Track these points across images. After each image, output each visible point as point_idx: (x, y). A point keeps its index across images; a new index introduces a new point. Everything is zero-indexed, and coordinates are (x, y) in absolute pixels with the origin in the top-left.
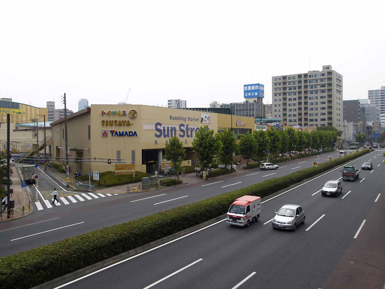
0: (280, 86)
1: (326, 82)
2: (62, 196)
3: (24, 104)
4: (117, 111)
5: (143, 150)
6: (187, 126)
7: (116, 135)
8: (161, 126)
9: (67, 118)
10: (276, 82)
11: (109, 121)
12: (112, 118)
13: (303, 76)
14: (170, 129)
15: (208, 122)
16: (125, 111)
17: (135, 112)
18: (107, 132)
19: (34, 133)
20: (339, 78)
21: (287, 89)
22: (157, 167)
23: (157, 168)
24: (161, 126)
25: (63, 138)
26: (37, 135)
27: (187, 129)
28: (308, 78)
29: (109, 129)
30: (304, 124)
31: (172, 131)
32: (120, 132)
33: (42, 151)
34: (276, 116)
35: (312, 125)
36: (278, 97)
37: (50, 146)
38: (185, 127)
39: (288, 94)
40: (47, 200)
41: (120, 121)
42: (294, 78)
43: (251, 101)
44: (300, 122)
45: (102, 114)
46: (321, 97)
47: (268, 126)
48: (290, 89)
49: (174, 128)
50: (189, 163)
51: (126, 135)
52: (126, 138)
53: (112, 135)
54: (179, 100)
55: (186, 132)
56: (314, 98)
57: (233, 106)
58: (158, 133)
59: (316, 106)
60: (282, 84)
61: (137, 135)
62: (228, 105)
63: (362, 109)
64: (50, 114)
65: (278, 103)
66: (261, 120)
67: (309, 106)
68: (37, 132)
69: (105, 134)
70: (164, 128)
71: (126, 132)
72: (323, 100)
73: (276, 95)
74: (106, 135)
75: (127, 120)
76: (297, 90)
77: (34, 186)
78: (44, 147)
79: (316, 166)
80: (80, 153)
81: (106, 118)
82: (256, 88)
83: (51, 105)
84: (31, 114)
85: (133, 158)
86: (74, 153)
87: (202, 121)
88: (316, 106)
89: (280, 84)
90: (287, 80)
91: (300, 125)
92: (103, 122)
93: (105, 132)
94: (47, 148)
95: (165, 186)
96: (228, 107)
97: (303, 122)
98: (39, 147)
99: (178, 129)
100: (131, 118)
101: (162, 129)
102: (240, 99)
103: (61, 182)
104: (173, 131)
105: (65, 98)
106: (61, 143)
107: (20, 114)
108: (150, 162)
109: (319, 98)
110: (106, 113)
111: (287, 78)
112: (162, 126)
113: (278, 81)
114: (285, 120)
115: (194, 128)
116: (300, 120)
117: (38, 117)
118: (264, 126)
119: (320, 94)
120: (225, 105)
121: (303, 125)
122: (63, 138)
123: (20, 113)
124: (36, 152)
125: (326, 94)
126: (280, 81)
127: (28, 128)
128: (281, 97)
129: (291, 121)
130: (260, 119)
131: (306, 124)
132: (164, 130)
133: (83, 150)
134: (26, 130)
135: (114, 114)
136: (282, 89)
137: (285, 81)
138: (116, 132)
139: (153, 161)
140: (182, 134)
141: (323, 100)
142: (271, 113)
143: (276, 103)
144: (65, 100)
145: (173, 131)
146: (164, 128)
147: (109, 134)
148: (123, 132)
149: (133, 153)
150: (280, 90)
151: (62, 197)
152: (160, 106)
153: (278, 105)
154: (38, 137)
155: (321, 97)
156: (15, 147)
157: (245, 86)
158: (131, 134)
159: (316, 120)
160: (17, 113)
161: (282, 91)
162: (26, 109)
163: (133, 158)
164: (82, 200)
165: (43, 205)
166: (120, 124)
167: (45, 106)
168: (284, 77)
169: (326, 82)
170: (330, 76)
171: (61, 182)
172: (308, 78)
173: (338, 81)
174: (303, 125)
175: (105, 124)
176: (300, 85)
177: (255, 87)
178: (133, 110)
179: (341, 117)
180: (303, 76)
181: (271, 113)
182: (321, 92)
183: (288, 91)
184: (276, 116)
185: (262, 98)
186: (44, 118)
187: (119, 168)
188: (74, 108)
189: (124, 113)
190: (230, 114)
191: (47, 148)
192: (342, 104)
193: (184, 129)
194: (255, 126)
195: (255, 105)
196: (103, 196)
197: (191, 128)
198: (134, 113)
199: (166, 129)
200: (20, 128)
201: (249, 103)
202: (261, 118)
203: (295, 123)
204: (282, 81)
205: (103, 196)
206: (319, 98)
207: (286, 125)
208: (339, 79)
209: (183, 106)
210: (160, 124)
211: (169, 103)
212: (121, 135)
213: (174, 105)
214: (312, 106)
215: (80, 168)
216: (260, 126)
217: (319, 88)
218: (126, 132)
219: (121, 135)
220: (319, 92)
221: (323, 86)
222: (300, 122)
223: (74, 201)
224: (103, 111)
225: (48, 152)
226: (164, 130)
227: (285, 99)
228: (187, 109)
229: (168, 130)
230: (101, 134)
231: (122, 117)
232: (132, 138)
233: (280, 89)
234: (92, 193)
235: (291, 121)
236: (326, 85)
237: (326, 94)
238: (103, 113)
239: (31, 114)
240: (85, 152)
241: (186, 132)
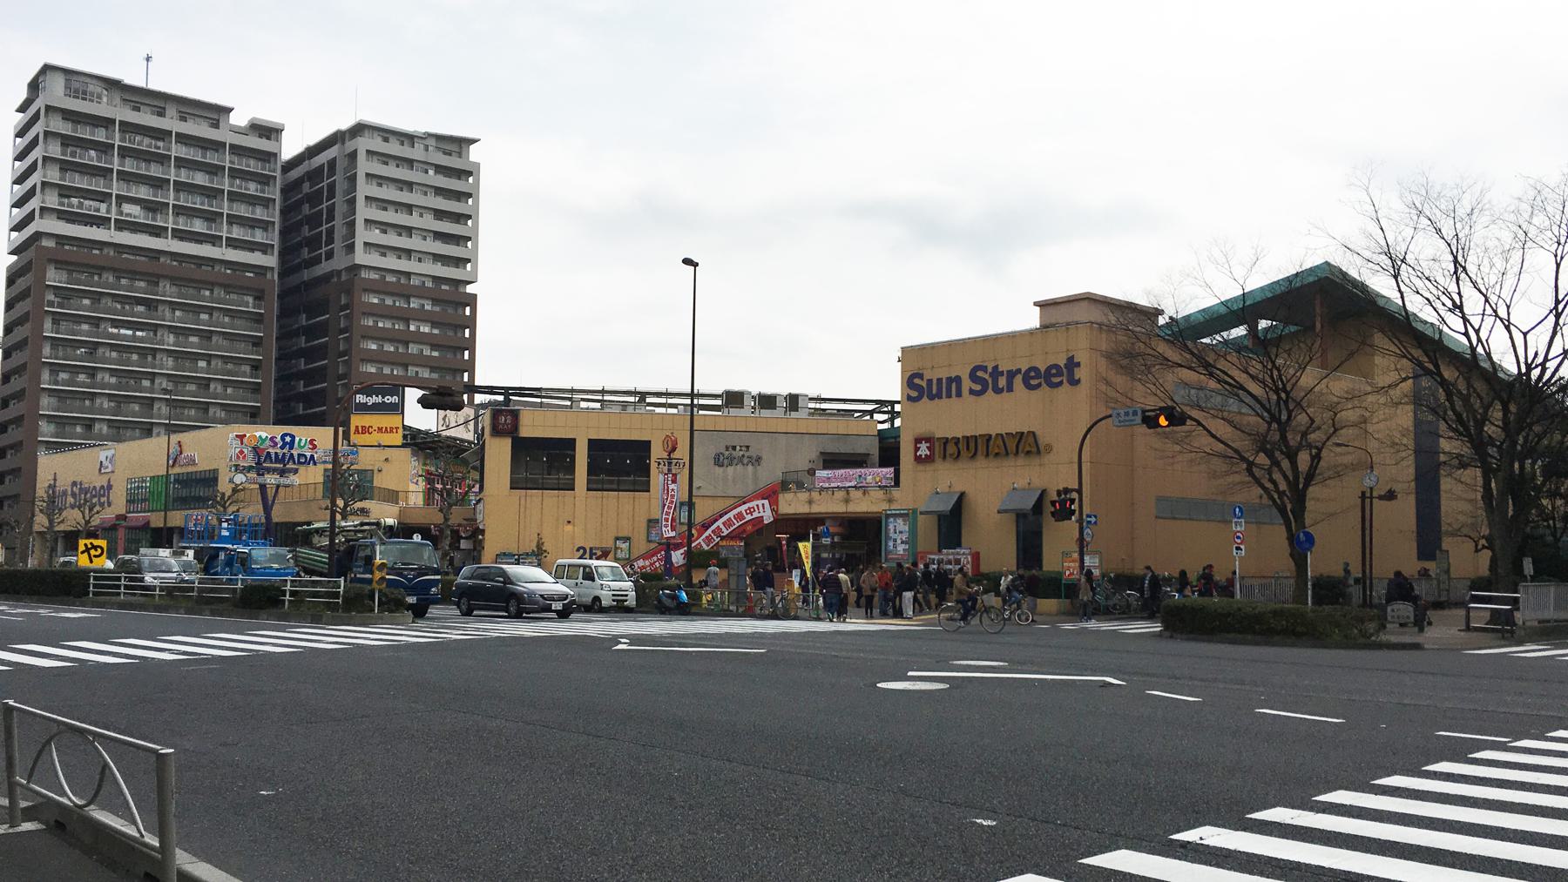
27: (996, 373)
70: (930, 381)
101: (924, 384)
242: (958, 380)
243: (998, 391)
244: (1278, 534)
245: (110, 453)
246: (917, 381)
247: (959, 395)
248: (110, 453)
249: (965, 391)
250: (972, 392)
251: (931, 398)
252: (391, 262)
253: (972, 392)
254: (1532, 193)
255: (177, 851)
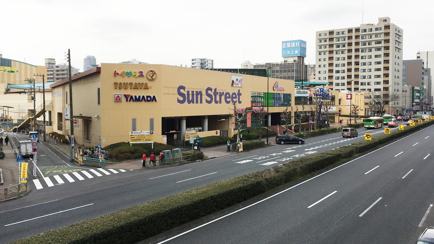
0: (325, 43)
1: (382, 37)
2: (66, 172)
3: (18, 61)
4: (133, 71)
5: (163, 119)
6: (215, 90)
7: (132, 100)
8: (184, 90)
9: (72, 79)
10: (320, 38)
11: (122, 83)
12: (126, 80)
13: (354, 31)
14: (195, 93)
15: (240, 85)
16: (142, 72)
17: (154, 73)
18: (120, 96)
19: (31, 96)
20: (398, 33)
21: (335, 46)
22: (180, 138)
23: (180, 139)
24: (184, 90)
25: (67, 103)
26: (33, 99)
27: (215, 93)
28: (361, 33)
29: (122, 93)
30: (355, 88)
31: (197, 95)
32: (135, 96)
33: (41, 118)
34: (319, 78)
35: (365, 90)
36: (322, 56)
37: (50, 112)
38: (213, 91)
39: (335, 52)
40: (48, 177)
41: (136, 83)
42: (343, 33)
43: (290, 60)
44: (349, 87)
45: (115, 75)
46: (376, 56)
47: (310, 90)
48: (338, 46)
49: (200, 92)
50: (217, 134)
51: (143, 100)
52: (143, 104)
53: (127, 101)
54: (204, 59)
55: (213, 96)
56: (367, 57)
57: (270, 66)
58: (181, 99)
59: (370, 67)
60: (328, 40)
61: (156, 101)
62: (262, 66)
63: (426, 71)
64: (50, 73)
65: (322, 63)
66: (302, 84)
67: (361, 67)
68: (34, 95)
69: (118, 99)
70: (188, 92)
71: (143, 97)
72: (378, 60)
73: (320, 54)
74: (120, 99)
75: (144, 83)
76: (347, 47)
77: (31, 159)
78: (43, 112)
79: (370, 139)
80: (87, 122)
81: (119, 80)
82: (296, 45)
83: (51, 63)
84: (26, 72)
85: (152, 128)
86: (80, 121)
87: (232, 84)
88: (370, 74)
89: (326, 41)
90: (335, 35)
91: (350, 89)
92: (116, 84)
93: (118, 97)
94: (47, 114)
95: (189, 160)
96: (262, 68)
97: (353, 86)
98: (37, 113)
99: (204, 93)
100: (150, 80)
101: (186, 93)
102: (276, 57)
103: (65, 155)
104: (199, 96)
105: (69, 54)
106: (64, 108)
107: (12, 74)
108: (171, 132)
109: (373, 57)
110: (120, 73)
111: (335, 33)
112: (186, 90)
113: (323, 37)
114: (331, 84)
115: (223, 92)
116: (349, 83)
117: (34, 77)
118: (306, 91)
119: (374, 53)
120: (259, 66)
121: (353, 89)
122: (67, 103)
123: (12, 72)
124: (32, 119)
125: (382, 52)
126: (325, 37)
127: (23, 91)
128: (327, 56)
129: (338, 84)
130: (301, 83)
131: (356, 89)
132: (188, 95)
133: (91, 118)
134: (20, 93)
135: (129, 74)
136: (328, 46)
137: (331, 36)
138: (132, 96)
139: (175, 131)
140: (209, 99)
141: (378, 60)
142: (315, 75)
143: (320, 63)
144: (69, 58)
145: (199, 96)
146: (188, 92)
147: (124, 99)
148: (139, 97)
149: (152, 121)
150: (326, 48)
151: (66, 173)
152: (184, 66)
153: (322, 66)
154: (35, 101)
155: (376, 56)
156: (7, 112)
157: (283, 42)
158: (149, 99)
159: (369, 84)
160: (8, 71)
161: (328, 49)
162: (20, 68)
163: (152, 128)
164: (90, 176)
165: (43, 182)
166: (137, 87)
167: (42, 63)
168: (331, 33)
169: (382, 37)
170: (387, 31)
171: (65, 155)
172: (361, 33)
173: (397, 36)
174: (353, 89)
175: (118, 87)
176: (350, 41)
177: (295, 44)
178: (152, 71)
179: (400, 81)
180: (354, 31)
181: (315, 75)
182: (376, 50)
183: (335, 48)
184: (319, 78)
185: (303, 58)
186: (43, 79)
187: (135, 139)
188: (79, 67)
189: (141, 74)
190: (265, 76)
191: (47, 114)
192: (401, 63)
193: (212, 94)
194: (296, 91)
195: (295, 66)
196: (115, 172)
197: (220, 93)
198: (152, 75)
199: (190, 93)
200: (12, 90)
201: (287, 63)
202: (302, 81)
203: (343, 87)
204: (328, 36)
205: (115, 172)
206: (373, 57)
207: (332, 89)
208: (399, 34)
209: (210, 66)
210: (184, 88)
211: (193, 62)
212: (137, 100)
213: (198, 65)
214: (364, 74)
215: (88, 139)
216: (301, 90)
217: (373, 45)
218: (143, 97)
219: (137, 100)
220: (373, 50)
221: (379, 42)
222: (349, 87)
223: (71, 180)
224: (115, 71)
225: (47, 119)
226: (188, 95)
227: (331, 58)
228: (215, 70)
229: (193, 95)
230: (113, 99)
231: (138, 78)
232: (151, 103)
233: (326, 46)
234: (103, 168)
235: (338, 84)
236: (383, 42)
237: (382, 52)
238: (116, 74)
239: (26, 72)
240: (94, 120)
241: (213, 96)
242: (200, 93)
243: (216, 102)
244: (348, 114)
245: (241, 77)
246: (182, 91)
247: (201, 102)
248: (241, 77)
249: (204, 101)
250: (207, 101)
251: (189, 102)
252: (22, 170)
253: (207, 101)
254: (382, 25)
255: (42, 188)
